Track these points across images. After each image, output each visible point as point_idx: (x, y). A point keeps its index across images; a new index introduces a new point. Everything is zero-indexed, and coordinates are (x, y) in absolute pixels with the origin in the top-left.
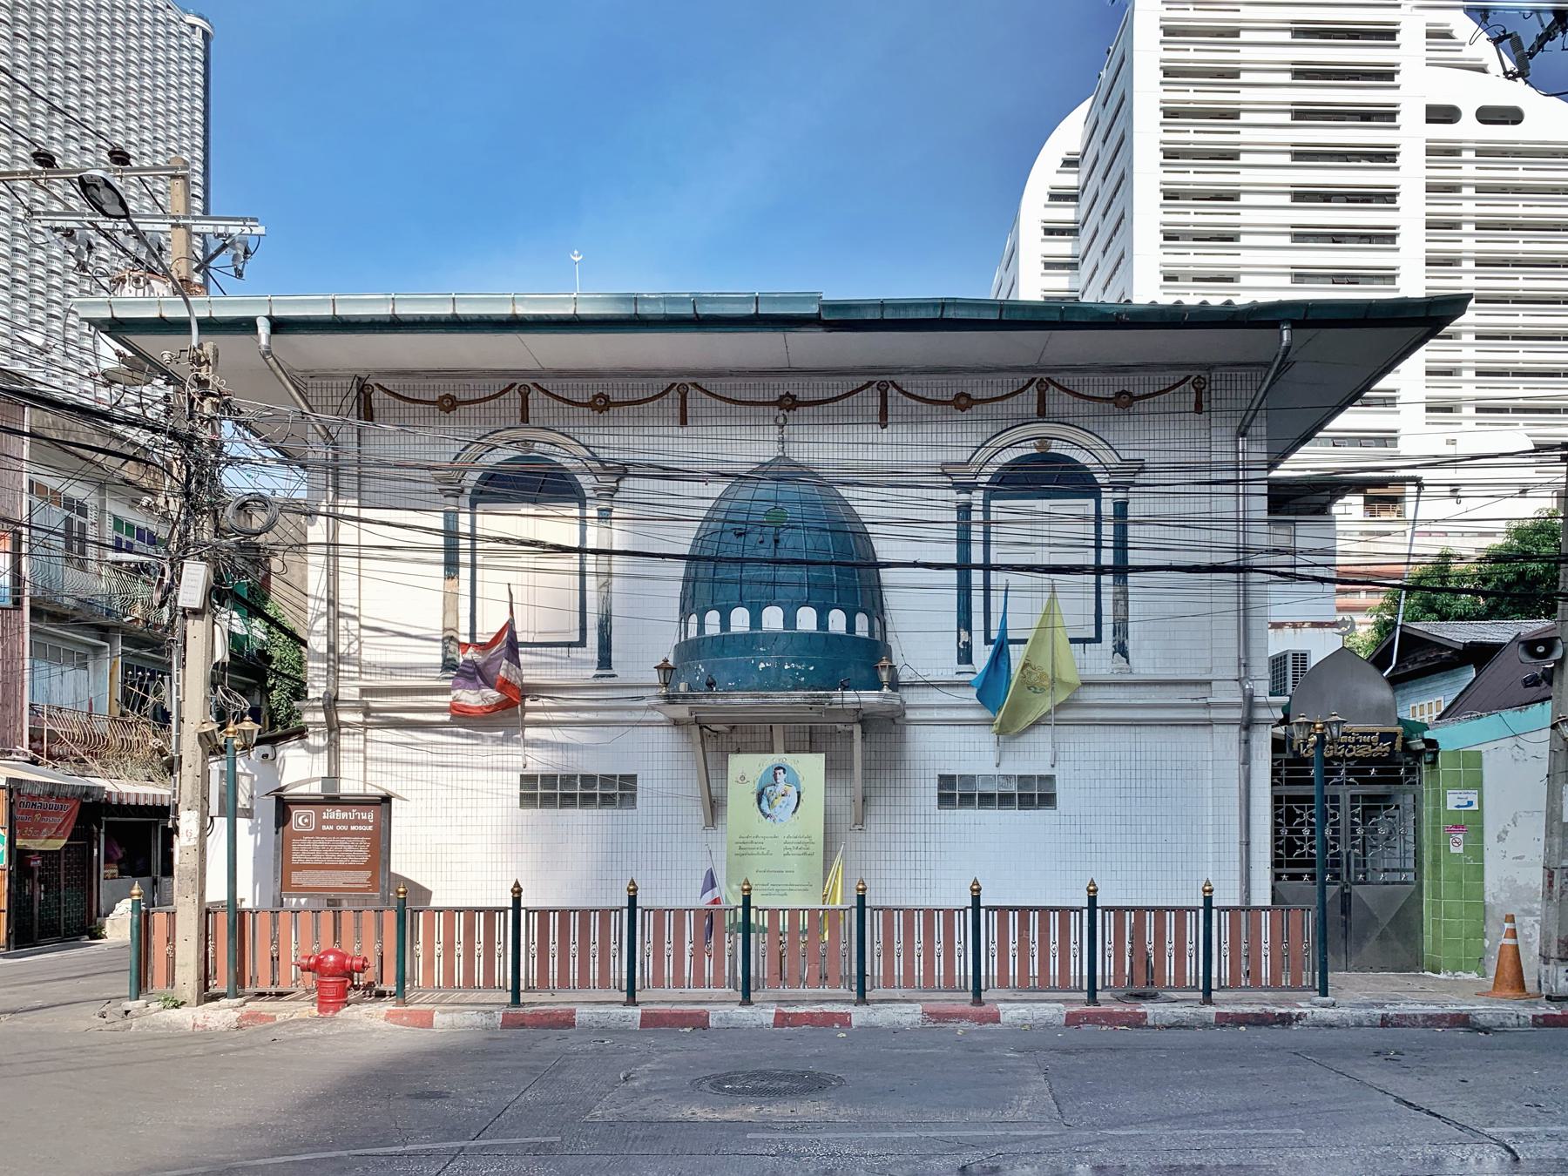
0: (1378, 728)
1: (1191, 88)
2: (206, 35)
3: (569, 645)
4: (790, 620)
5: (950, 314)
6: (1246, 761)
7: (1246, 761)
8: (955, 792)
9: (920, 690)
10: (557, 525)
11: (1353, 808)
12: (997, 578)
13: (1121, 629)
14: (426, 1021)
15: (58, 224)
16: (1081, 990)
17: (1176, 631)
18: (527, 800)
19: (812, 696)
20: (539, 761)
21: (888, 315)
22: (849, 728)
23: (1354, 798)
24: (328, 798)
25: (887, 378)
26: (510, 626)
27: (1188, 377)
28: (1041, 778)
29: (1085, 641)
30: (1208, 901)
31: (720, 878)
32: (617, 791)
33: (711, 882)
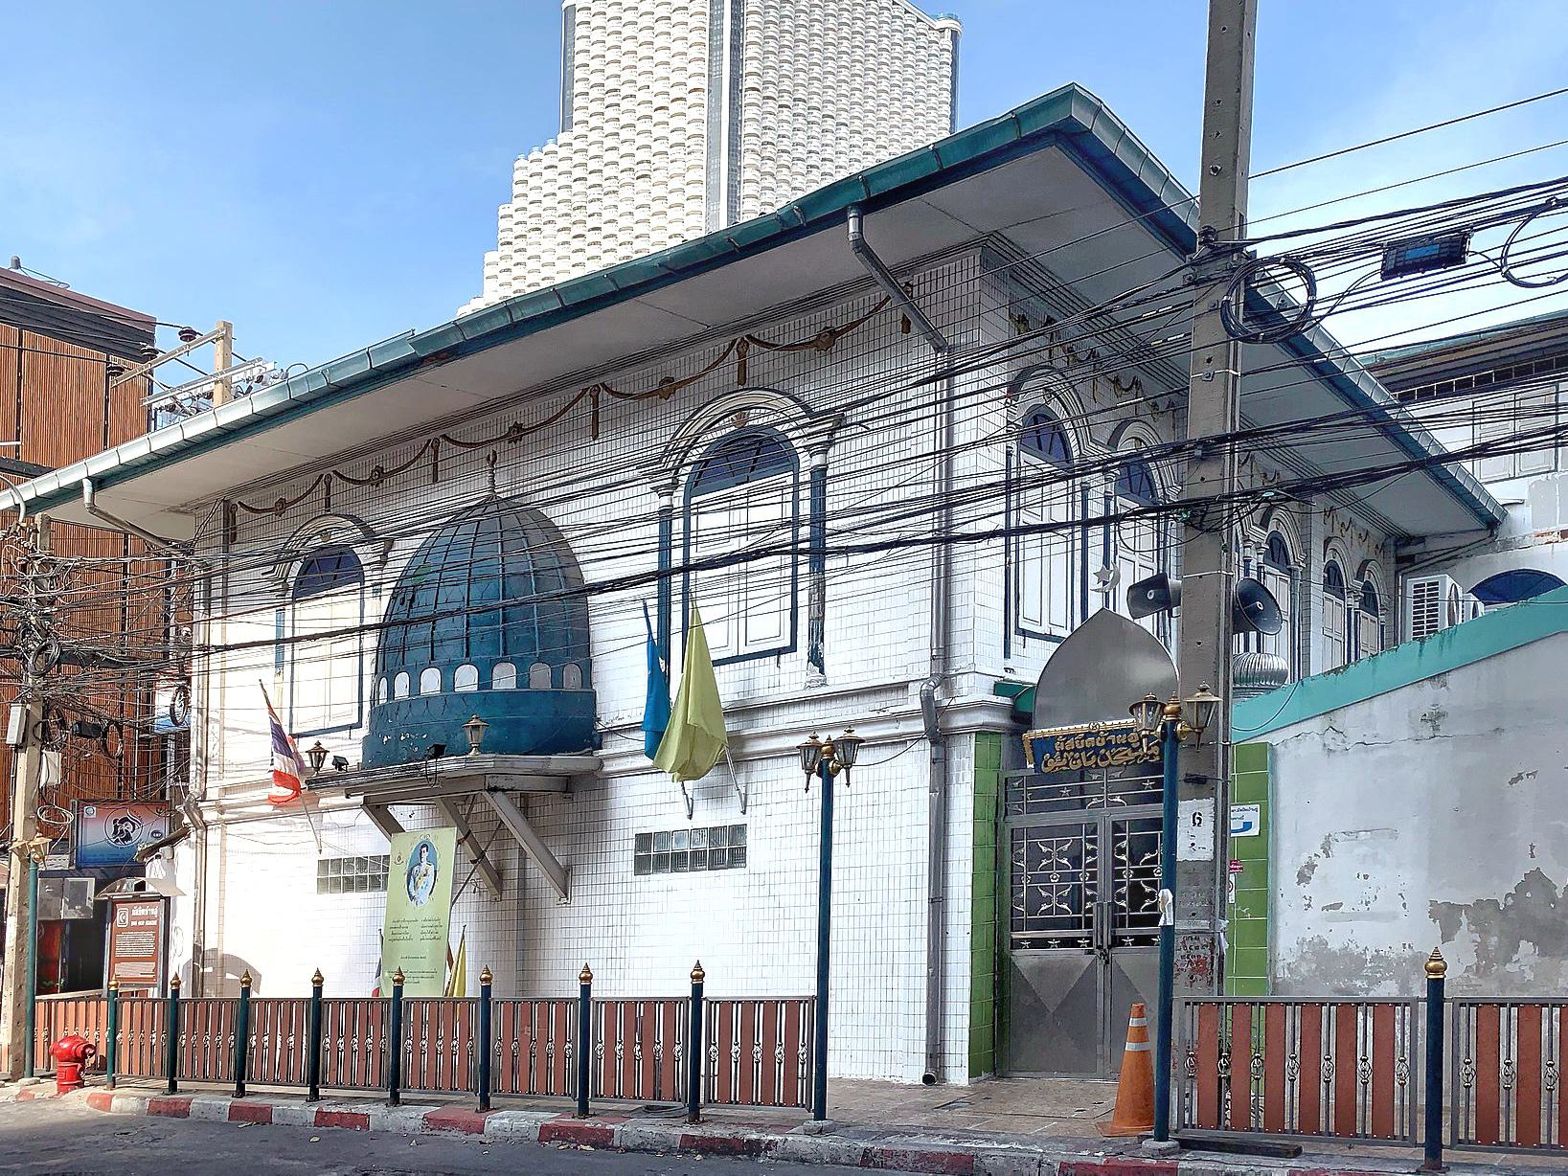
2: (954, 34)
11: (1117, 840)
13: (817, 633)
18: (325, 885)
22: (1027, 746)
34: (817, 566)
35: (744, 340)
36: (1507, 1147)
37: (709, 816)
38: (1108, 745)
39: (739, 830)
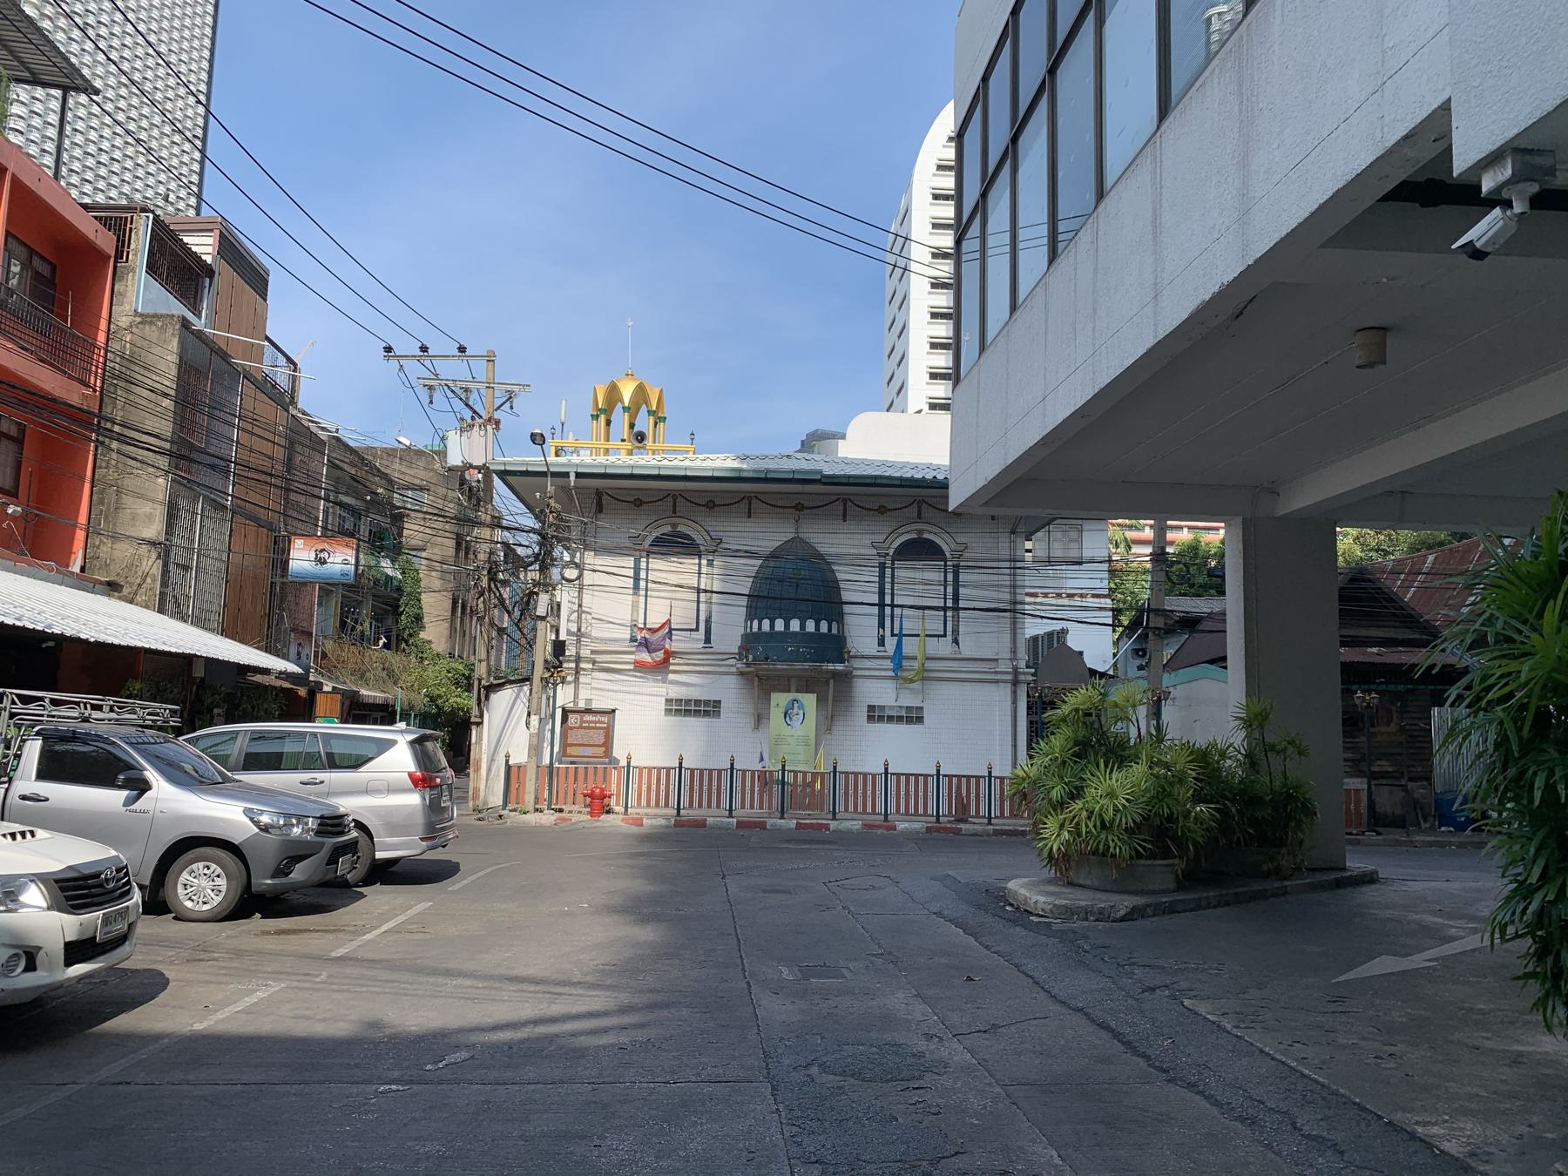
6: (1014, 702)
7: (1014, 702)
12: (897, 611)
13: (956, 631)
17: (983, 639)
18: (668, 712)
20: (676, 692)
31: (766, 756)
33: (762, 759)
34: (956, 619)
37: (909, 700)
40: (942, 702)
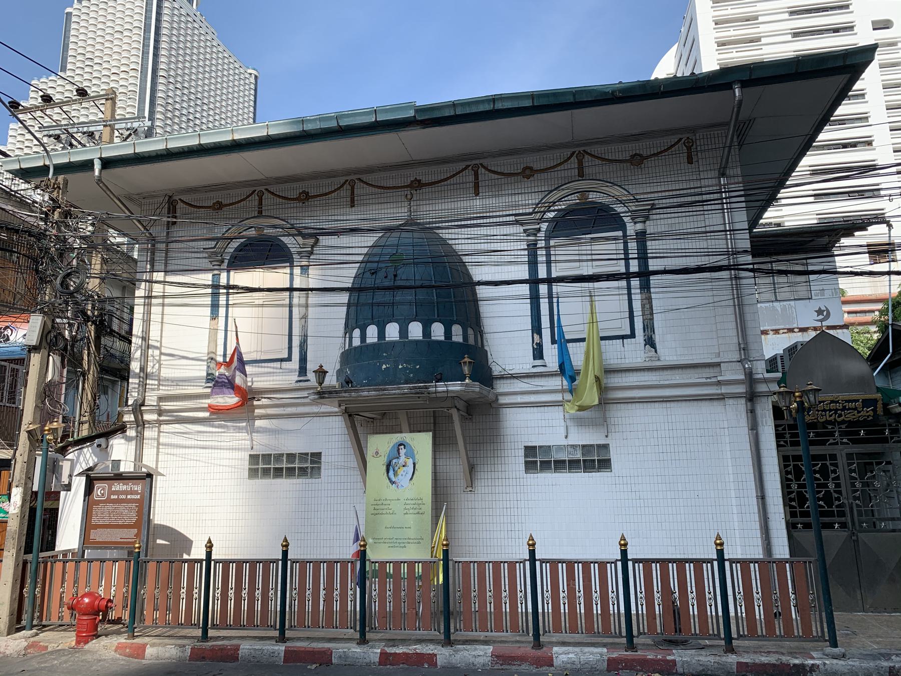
0: (860, 396)
1: (732, 29)
2: (256, 77)
3: (282, 360)
4: (404, 332)
5: (499, 106)
7: (754, 427)
8: (538, 460)
9: (508, 381)
10: (277, 277)
11: (850, 464)
13: (649, 327)
14: (140, 652)
15: (51, 133)
16: (621, 636)
17: (689, 324)
18: (253, 473)
19: (415, 388)
20: (263, 444)
21: (459, 111)
23: (849, 456)
24: (116, 475)
25: (477, 162)
26: (237, 350)
27: (681, 139)
28: (599, 446)
29: (623, 337)
30: (720, 553)
32: (309, 465)
34: (645, 287)
35: (580, 155)
36: (762, 637)
38: (844, 409)
39: (606, 447)
40: (636, 435)
